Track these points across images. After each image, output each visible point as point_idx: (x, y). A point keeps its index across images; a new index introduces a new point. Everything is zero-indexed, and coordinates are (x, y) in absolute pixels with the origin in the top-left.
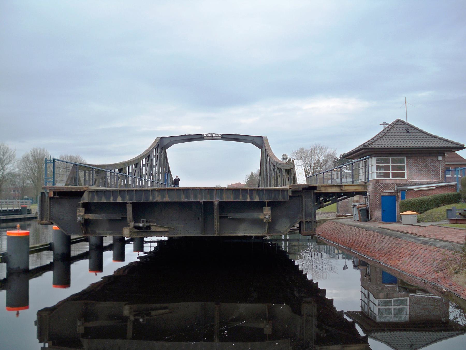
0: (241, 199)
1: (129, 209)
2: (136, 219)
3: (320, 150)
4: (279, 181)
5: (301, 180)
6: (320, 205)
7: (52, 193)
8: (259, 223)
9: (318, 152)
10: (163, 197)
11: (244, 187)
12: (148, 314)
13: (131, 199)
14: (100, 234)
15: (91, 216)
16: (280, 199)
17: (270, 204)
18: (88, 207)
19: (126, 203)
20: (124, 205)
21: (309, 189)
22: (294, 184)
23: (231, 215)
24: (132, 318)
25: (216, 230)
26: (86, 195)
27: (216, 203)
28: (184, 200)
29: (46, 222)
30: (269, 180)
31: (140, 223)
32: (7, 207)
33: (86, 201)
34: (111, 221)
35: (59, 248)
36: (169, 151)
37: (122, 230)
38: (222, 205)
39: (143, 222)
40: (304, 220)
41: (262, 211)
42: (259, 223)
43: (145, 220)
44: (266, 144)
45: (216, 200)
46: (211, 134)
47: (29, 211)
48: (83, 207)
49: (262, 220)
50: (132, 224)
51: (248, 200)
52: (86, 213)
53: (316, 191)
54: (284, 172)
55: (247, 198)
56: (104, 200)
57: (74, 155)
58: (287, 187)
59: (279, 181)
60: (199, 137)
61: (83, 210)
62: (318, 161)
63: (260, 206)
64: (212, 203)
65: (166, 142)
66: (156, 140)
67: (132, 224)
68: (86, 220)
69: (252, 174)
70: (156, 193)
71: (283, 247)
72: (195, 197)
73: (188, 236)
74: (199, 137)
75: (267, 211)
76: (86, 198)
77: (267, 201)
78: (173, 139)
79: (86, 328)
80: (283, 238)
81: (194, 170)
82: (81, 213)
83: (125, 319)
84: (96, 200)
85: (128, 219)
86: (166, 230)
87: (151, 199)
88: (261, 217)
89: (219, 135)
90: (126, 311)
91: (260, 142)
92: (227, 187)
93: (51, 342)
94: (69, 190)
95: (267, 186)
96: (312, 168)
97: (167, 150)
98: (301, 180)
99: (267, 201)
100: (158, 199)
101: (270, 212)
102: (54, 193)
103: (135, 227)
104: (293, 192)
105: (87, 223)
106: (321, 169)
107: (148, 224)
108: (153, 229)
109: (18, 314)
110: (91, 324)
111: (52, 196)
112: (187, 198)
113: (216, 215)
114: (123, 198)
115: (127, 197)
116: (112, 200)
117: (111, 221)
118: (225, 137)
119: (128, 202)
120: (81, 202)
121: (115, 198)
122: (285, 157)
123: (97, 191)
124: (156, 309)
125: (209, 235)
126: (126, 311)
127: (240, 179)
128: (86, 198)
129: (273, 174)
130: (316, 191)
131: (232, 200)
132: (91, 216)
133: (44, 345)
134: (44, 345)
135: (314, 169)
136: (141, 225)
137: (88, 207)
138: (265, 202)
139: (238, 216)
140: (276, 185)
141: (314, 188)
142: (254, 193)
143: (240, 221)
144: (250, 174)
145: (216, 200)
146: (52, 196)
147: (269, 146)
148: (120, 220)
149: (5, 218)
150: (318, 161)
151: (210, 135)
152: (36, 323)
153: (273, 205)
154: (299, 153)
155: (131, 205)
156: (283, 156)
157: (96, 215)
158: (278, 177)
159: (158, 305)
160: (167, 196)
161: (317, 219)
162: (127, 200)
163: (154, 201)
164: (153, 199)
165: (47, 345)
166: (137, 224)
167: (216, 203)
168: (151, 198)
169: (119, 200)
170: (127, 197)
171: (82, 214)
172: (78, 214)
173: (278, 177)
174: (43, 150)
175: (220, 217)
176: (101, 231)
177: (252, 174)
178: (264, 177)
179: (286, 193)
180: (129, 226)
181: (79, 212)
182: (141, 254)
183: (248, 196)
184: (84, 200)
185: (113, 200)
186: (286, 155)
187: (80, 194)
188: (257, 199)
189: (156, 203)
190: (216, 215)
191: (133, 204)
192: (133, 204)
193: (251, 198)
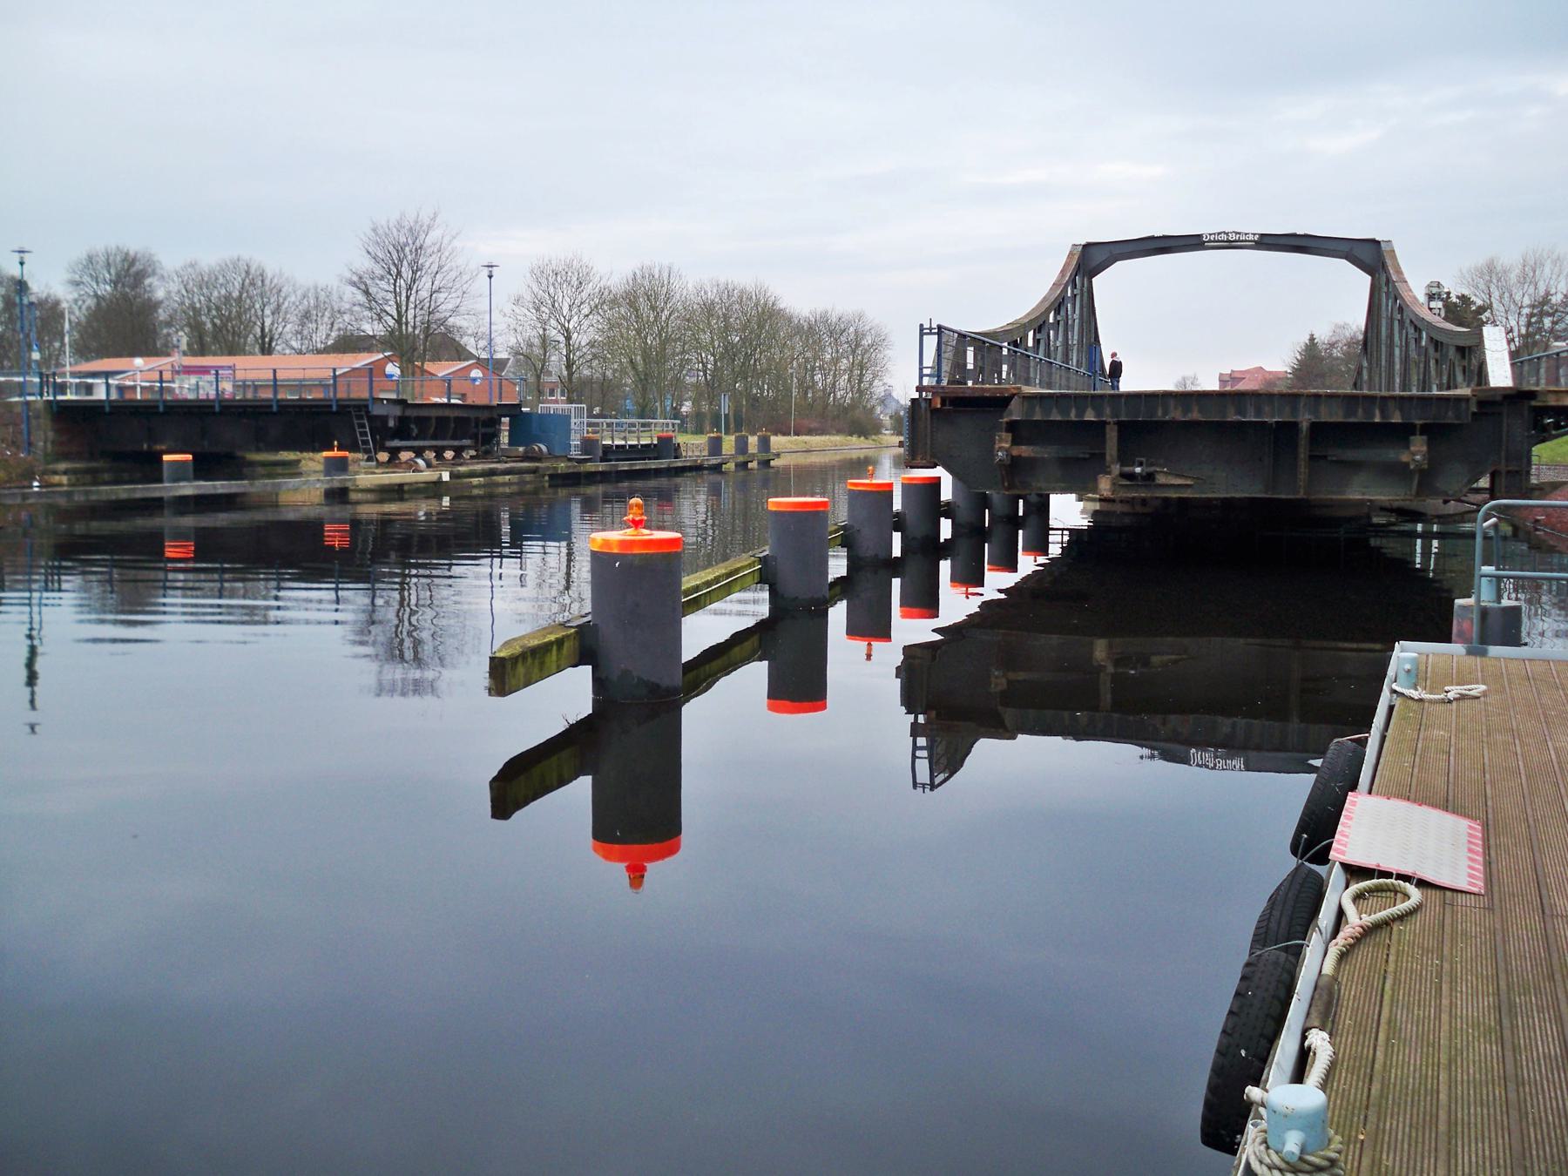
0: (1359, 417)
1: (1112, 435)
2: (1125, 458)
3: (1555, 262)
4: (1433, 373)
5: (1500, 374)
6: (1544, 435)
7: (938, 401)
8: (1399, 472)
9: (1547, 270)
10: (1186, 411)
11: (1281, 388)
12: (1146, 664)
13: (1115, 414)
15: (1025, 451)
16: (1450, 418)
17: (1425, 429)
19: (1105, 423)
20: (1100, 426)
21: (1515, 398)
22: (1479, 384)
23: (1336, 453)
24: (1111, 669)
25: (1300, 485)
27: (1305, 426)
28: (1233, 417)
30: (1397, 367)
31: (1133, 465)
32: (625, 439)
36: (1102, 284)
37: (1096, 481)
38: (1316, 428)
39: (1141, 464)
40: (1503, 468)
41: (1407, 447)
42: (1399, 472)
44: (1389, 262)
45: (1305, 419)
47: (676, 451)
48: (1007, 431)
49: (1407, 465)
50: (1116, 469)
51: (1377, 420)
52: (1015, 442)
53: (1534, 403)
54: (1452, 353)
55: (1373, 416)
56: (1056, 416)
57: (743, 278)
58: (1464, 391)
59: (1433, 373)
61: (1009, 436)
62: (1545, 300)
63: (1402, 434)
64: (1294, 426)
66: (1071, 254)
67: (1116, 469)
69: (1312, 339)
71: (1418, 560)
72: (1258, 412)
73: (1237, 495)
75: (1417, 451)
76: (1015, 412)
77: (1418, 422)
78: (1117, 250)
79: (1009, 682)
80: (1419, 541)
81: (1172, 340)
82: (1003, 446)
87: (1159, 415)
88: (1405, 458)
91: (1370, 256)
92: (1212, 385)
93: (933, 713)
95: (1390, 386)
96: (1523, 321)
98: (1500, 374)
99: (1418, 422)
100: (1176, 414)
101: (1425, 448)
103: (1123, 475)
104: (1481, 403)
105: (1015, 467)
106: (1554, 323)
107: (1152, 469)
108: (1161, 479)
112: (1239, 412)
113: (1303, 452)
114: (1099, 413)
115: (1108, 411)
116: (1073, 416)
117: (1065, 462)
118: (1267, 242)
121: (1081, 412)
122: (1435, 290)
125: (1283, 496)
126: (1100, 650)
127: (1270, 356)
128: (1015, 412)
129: (1413, 355)
130: (1534, 403)
131: (1340, 420)
132: (1025, 451)
133: (916, 718)
134: (916, 718)
135: (1529, 324)
136: (1138, 470)
138: (1414, 426)
139: (1350, 455)
140: (1425, 385)
141: (1532, 395)
142: (1391, 404)
143: (1356, 466)
144: (1306, 339)
145: (1305, 419)
147: (1399, 272)
149: (124, 496)
150: (1545, 300)
152: (899, 672)
153: (1434, 432)
154: (1482, 273)
156: (1429, 286)
157: (1037, 449)
158: (1432, 363)
160: (1196, 409)
161: (1534, 481)
162: (1107, 416)
164: (1165, 413)
165: (921, 719)
166: (1127, 469)
167: (1305, 426)
168: (1160, 413)
169: (1090, 416)
173: (1432, 363)
175: (1311, 457)
177: (1312, 339)
178: (1379, 359)
179: (1463, 405)
182: (1042, 560)
183: (1377, 412)
186: (1439, 285)
187: (1000, 402)
188: (1396, 418)
189: (1174, 422)
190: (1303, 452)
192: (1119, 423)
193: (1383, 415)
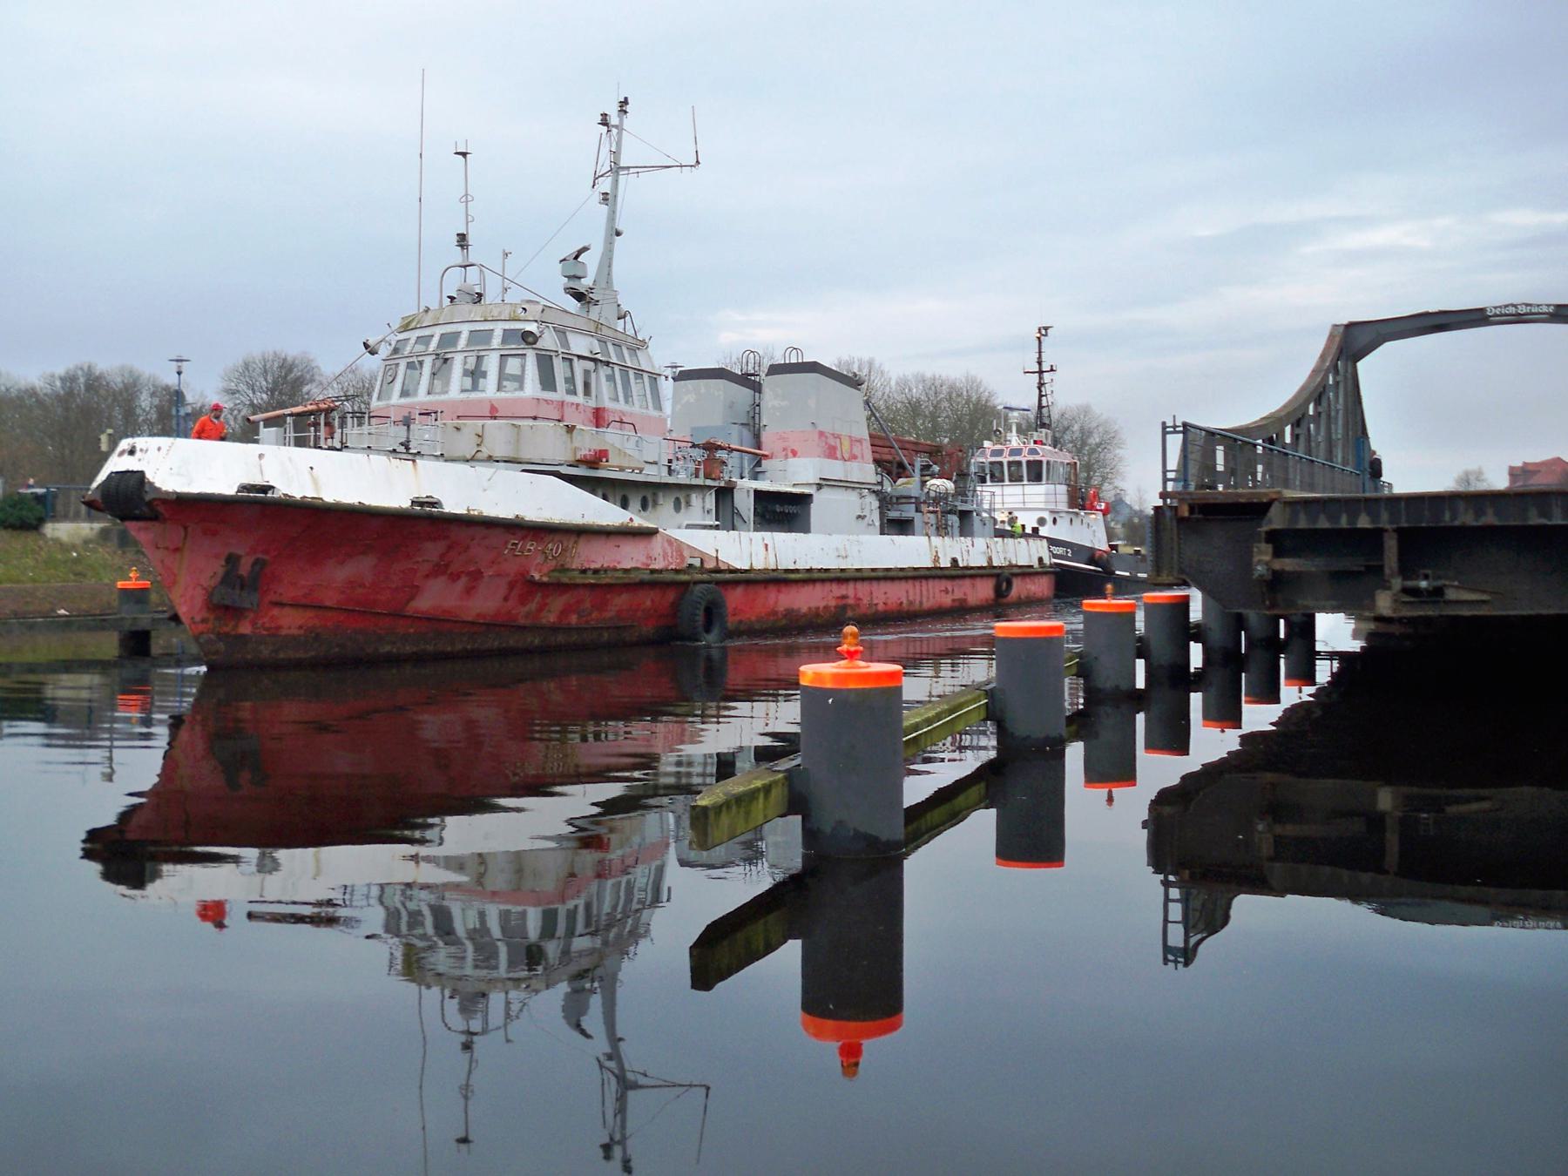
1: (1391, 545)
2: (1406, 570)
10: (1479, 513)
14: (1307, 607)
15: (1288, 564)
18: (1280, 542)
20: (1376, 535)
26: (1274, 511)
29: (1171, 579)
31: (1417, 578)
33: (1277, 525)
34: (1337, 576)
35: (1162, 650)
39: (1426, 577)
43: (1429, 572)
46: (1515, 306)
50: (1397, 583)
56: (1323, 523)
60: (1475, 318)
61: (1269, 548)
65: (1362, 339)
67: (1397, 583)
68: (1275, 573)
70: (1461, 505)
73: (1544, 612)
74: (1475, 318)
76: (1276, 519)
82: (1263, 560)
83: (1376, 821)
84: (1302, 524)
85: (1387, 571)
86: (1485, 597)
89: (1545, 309)
90: (1385, 799)
94: (1230, 501)
97: (1360, 365)
100: (1467, 518)
102: (1192, 509)
103: (1405, 591)
105: (1277, 581)
107: (1439, 583)
109: (1110, 800)
110: (1290, 830)
111: (1186, 514)
114: (1375, 517)
115: (1385, 516)
116: (1344, 523)
117: (1337, 576)
119: (1388, 526)
120: (1265, 528)
123: (1306, 502)
124: (1458, 801)
126: (1385, 799)
132: (1288, 564)
136: (1423, 584)
137: (1280, 542)
146: (1186, 514)
148: (1359, 572)
151: (1512, 310)
155: (1395, 536)
157: (1301, 561)
159: (1467, 792)
162: (1385, 521)
163: (1457, 523)
164: (1454, 518)
166: (1410, 583)
168: (1447, 517)
169: (1364, 522)
170: (1385, 516)
171: (1267, 558)
172: (1256, 559)
174: (871, 364)
176: (1309, 602)
180: (1389, 588)
181: (1260, 552)
184: (1270, 522)
185: (1349, 522)
187: (1256, 510)
189: (1464, 530)
191: (1400, 532)
192: (1400, 532)
